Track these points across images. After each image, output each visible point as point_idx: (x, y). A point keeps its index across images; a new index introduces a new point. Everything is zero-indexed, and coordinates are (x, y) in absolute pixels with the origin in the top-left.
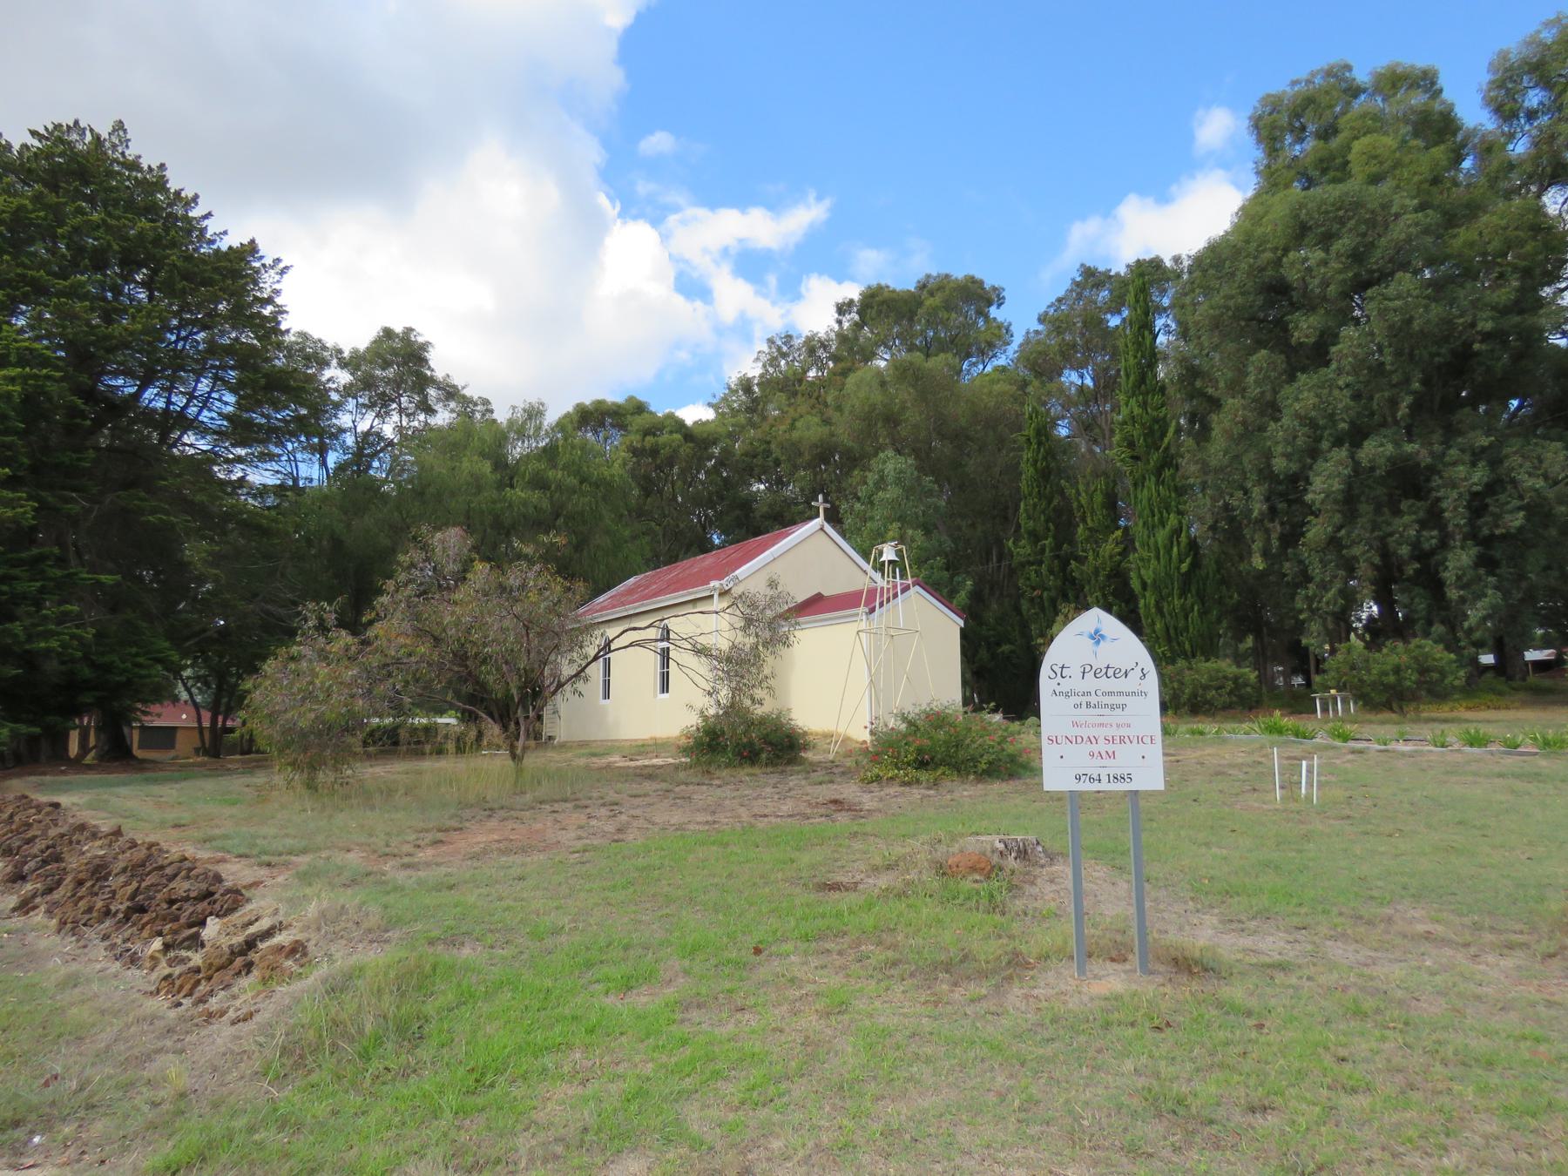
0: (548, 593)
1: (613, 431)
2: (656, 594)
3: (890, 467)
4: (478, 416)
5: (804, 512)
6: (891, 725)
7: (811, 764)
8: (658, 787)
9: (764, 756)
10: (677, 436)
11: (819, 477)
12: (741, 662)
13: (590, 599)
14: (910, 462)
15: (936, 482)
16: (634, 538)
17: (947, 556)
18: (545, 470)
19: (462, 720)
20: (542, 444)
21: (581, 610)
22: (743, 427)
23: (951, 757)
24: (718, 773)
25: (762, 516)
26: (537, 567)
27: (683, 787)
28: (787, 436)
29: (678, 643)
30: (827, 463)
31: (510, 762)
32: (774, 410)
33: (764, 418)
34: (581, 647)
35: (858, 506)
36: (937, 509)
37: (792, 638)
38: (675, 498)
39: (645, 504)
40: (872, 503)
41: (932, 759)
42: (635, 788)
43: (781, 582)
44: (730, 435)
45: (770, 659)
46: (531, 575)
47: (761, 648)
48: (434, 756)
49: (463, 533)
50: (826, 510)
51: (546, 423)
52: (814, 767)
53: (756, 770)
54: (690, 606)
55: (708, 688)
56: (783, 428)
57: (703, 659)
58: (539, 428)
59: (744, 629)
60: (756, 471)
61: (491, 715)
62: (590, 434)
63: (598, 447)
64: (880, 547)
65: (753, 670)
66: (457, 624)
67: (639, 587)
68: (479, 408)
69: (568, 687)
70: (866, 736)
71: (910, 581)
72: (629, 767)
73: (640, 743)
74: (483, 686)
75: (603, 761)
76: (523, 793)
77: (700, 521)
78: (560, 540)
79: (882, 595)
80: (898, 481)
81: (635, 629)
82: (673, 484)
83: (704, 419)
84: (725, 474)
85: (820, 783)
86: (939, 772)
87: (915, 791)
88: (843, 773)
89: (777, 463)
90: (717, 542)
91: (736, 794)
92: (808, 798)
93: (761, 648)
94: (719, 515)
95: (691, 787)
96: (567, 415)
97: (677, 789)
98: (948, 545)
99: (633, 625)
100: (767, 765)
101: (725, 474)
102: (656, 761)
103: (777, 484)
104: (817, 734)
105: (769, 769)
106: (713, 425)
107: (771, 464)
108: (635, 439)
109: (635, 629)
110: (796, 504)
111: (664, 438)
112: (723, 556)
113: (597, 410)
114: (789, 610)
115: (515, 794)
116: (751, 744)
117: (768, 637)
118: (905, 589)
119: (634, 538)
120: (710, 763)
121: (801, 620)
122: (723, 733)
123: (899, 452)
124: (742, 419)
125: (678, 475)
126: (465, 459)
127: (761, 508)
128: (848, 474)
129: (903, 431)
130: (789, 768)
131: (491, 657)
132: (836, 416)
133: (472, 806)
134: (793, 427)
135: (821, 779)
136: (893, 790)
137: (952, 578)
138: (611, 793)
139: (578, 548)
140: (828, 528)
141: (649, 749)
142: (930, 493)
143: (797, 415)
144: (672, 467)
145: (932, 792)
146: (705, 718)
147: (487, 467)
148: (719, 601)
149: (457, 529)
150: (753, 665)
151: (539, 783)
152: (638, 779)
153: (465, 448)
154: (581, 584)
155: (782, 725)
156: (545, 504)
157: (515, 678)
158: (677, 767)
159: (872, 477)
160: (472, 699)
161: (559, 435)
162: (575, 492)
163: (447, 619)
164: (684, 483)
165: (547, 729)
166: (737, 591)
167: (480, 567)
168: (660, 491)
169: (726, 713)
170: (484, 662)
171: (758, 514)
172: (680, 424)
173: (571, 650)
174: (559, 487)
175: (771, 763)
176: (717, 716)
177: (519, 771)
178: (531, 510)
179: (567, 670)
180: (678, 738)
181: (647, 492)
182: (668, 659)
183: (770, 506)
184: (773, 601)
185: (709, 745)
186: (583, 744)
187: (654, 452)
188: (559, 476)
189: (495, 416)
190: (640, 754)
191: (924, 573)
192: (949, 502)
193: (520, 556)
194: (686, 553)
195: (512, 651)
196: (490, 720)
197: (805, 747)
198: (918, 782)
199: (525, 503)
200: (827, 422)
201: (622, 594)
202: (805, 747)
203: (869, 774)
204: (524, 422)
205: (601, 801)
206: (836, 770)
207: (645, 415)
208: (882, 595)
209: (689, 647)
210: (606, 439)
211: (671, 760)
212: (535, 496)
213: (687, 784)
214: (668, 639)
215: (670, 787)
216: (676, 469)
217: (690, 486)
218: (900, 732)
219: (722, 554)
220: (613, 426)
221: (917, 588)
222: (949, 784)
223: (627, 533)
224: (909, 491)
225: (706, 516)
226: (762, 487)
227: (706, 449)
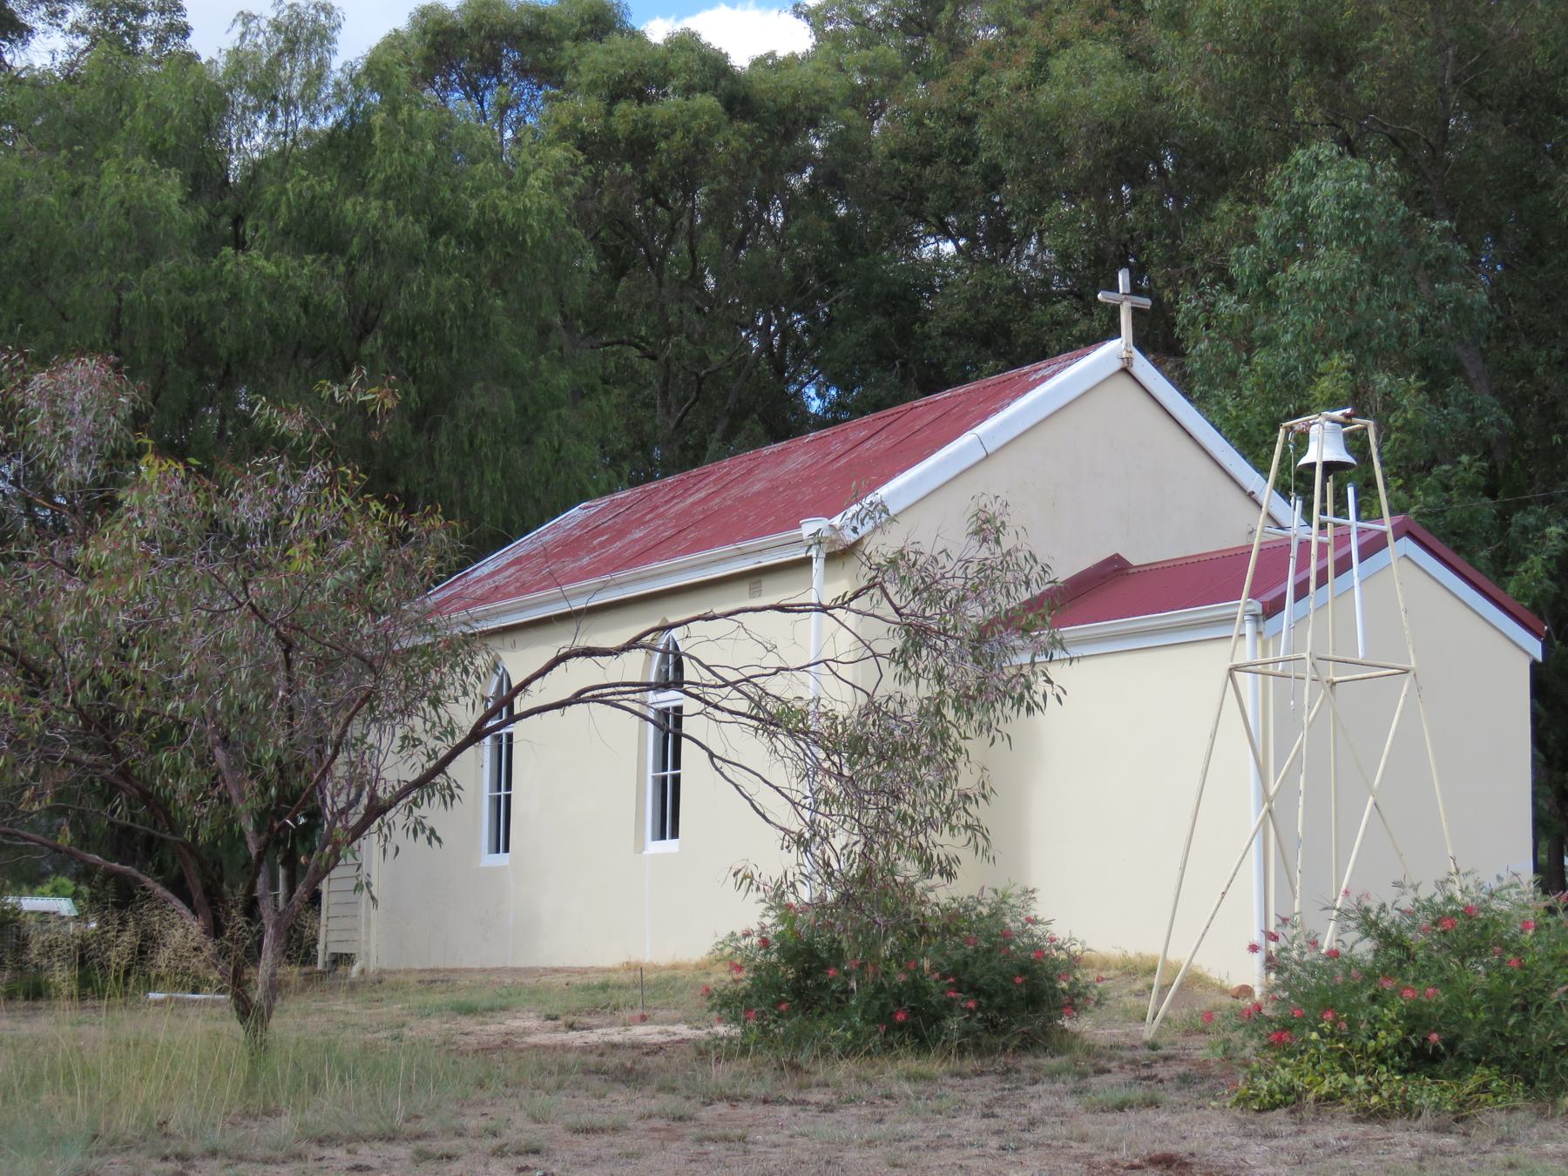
0: (345, 546)
1: (524, 88)
2: (645, 554)
3: (1326, 185)
4: (146, 44)
5: (1068, 323)
6: (1327, 943)
7: (1090, 1051)
8: (654, 1105)
9: (953, 1024)
10: (707, 102)
11: (1113, 220)
12: (891, 753)
13: (463, 565)
14: (1382, 176)
15: (1458, 235)
16: (579, 394)
17: (1488, 453)
18: (331, 197)
19: (94, 903)
20: (326, 123)
21: (436, 596)
22: (894, 75)
23: (1506, 1041)
24: (821, 1071)
25: (948, 333)
26: (317, 472)
27: (722, 1108)
28: (1023, 98)
29: (713, 695)
30: (1136, 176)
31: (233, 1026)
32: (987, 24)
33: (957, 49)
34: (435, 703)
35: (1227, 304)
36: (1461, 310)
37: (1040, 685)
38: (697, 279)
39: (610, 296)
40: (1270, 296)
41: (1451, 1044)
42: (587, 1108)
43: (1013, 521)
44: (856, 98)
45: (975, 746)
46: (298, 494)
47: (950, 713)
48: (21, 1004)
49: (108, 374)
50: (1137, 312)
51: (336, 63)
52: (1098, 1060)
53: (933, 1065)
54: (571, 627)
55: (796, 826)
56: (1011, 76)
57: (784, 741)
58: (317, 77)
59: (900, 657)
60: (933, 201)
61: (178, 887)
62: (456, 96)
63: (482, 135)
64: (1298, 423)
65: (928, 774)
66: (91, 631)
67: (597, 532)
68: (148, 21)
69: (397, 816)
70: (1250, 973)
71: (1387, 525)
72: (566, 1048)
73: (596, 980)
74: (157, 805)
75: (492, 1029)
76: (272, 1113)
77: (767, 346)
78: (380, 397)
79: (1303, 563)
80: (1348, 231)
81: (589, 652)
82: (692, 236)
83: (782, 53)
84: (842, 211)
85: (1121, 1107)
86: (1472, 1082)
87: (1399, 1136)
88: (1185, 1080)
89: (993, 178)
90: (815, 405)
91: (874, 1130)
92: (1087, 1148)
93: (950, 713)
94: (823, 332)
95: (745, 1109)
96: (394, 42)
97: (706, 1114)
98: (1494, 417)
99: (585, 641)
100: (962, 1050)
101: (842, 211)
102: (640, 1032)
103: (991, 241)
104: (1106, 964)
105: (971, 1063)
106: (808, 70)
107: (975, 181)
108: (583, 107)
109: (589, 652)
110: (1047, 298)
111: (668, 106)
112: (837, 447)
113: (477, 25)
114: (1031, 605)
115: (246, 1114)
116: (917, 987)
117: (971, 681)
118: (1372, 547)
119: (579, 394)
120: (798, 1045)
121: (1068, 632)
122: (838, 954)
123: (1350, 146)
124: (891, 50)
125: (709, 214)
126: (110, 166)
127: (942, 311)
128: (1201, 210)
129: (1366, 85)
130: (1028, 1061)
131: (182, 727)
132: (1164, 42)
133: (128, 1146)
134: (1040, 71)
135: (1123, 1094)
136: (1335, 1130)
137: (1504, 517)
138: (520, 1120)
139: (423, 418)
140: (1144, 367)
141: (620, 997)
142: (1441, 268)
143: (1051, 41)
144: (689, 192)
145: (1449, 1141)
146: (787, 913)
147: (170, 188)
148: (827, 579)
149: (91, 363)
150: (928, 760)
151: (316, 1086)
152: (595, 1082)
153: (110, 132)
154: (437, 521)
155: (1007, 936)
156: (333, 295)
157: (251, 787)
158: (702, 1052)
159: (1268, 222)
160: (123, 842)
161: (375, 99)
162: (415, 260)
163: (65, 619)
164: (725, 241)
165: (329, 936)
166: (882, 546)
167: (150, 468)
168: (655, 262)
169: (846, 898)
170: (161, 740)
171: (934, 327)
172: (714, 67)
173: (406, 711)
174: (373, 247)
175: (972, 1045)
176: (820, 906)
177: (259, 1049)
178: (293, 311)
179: (397, 769)
180: (703, 968)
181: (618, 266)
182: (678, 739)
183: (971, 302)
184: (985, 579)
185: (798, 992)
186: (434, 980)
187: (640, 146)
188: (374, 213)
189: (195, 43)
190: (594, 1011)
191: (1423, 499)
192: (1497, 295)
193: (263, 442)
194: (727, 437)
195: (243, 709)
196: (177, 903)
197: (1075, 1001)
198: (1409, 1110)
199: (275, 290)
200: (1139, 59)
201: (547, 554)
202: (1075, 1001)
203: (1263, 1084)
204: (276, 61)
205: (495, 1142)
206: (1161, 1070)
207: (616, 40)
208: (1303, 563)
209: (744, 706)
210: (503, 109)
211: (684, 1031)
212: (302, 270)
213: (733, 1100)
214: (678, 683)
215: (688, 1107)
216: (700, 197)
217: (741, 244)
218: (1354, 963)
219: (836, 440)
220: (523, 71)
221: (1407, 545)
222: (1501, 1117)
223: (563, 379)
224: (1380, 259)
225: (786, 331)
226: (948, 248)
227: (788, 137)
